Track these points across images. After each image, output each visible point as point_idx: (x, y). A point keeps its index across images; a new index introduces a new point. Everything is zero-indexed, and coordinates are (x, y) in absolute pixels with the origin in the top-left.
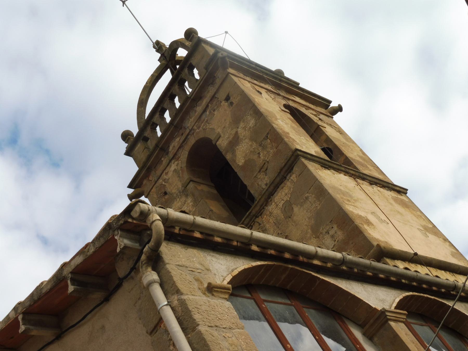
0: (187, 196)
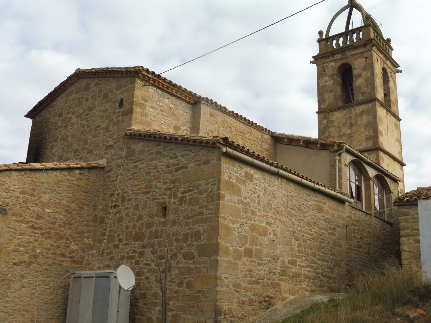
0: (332, 79)
